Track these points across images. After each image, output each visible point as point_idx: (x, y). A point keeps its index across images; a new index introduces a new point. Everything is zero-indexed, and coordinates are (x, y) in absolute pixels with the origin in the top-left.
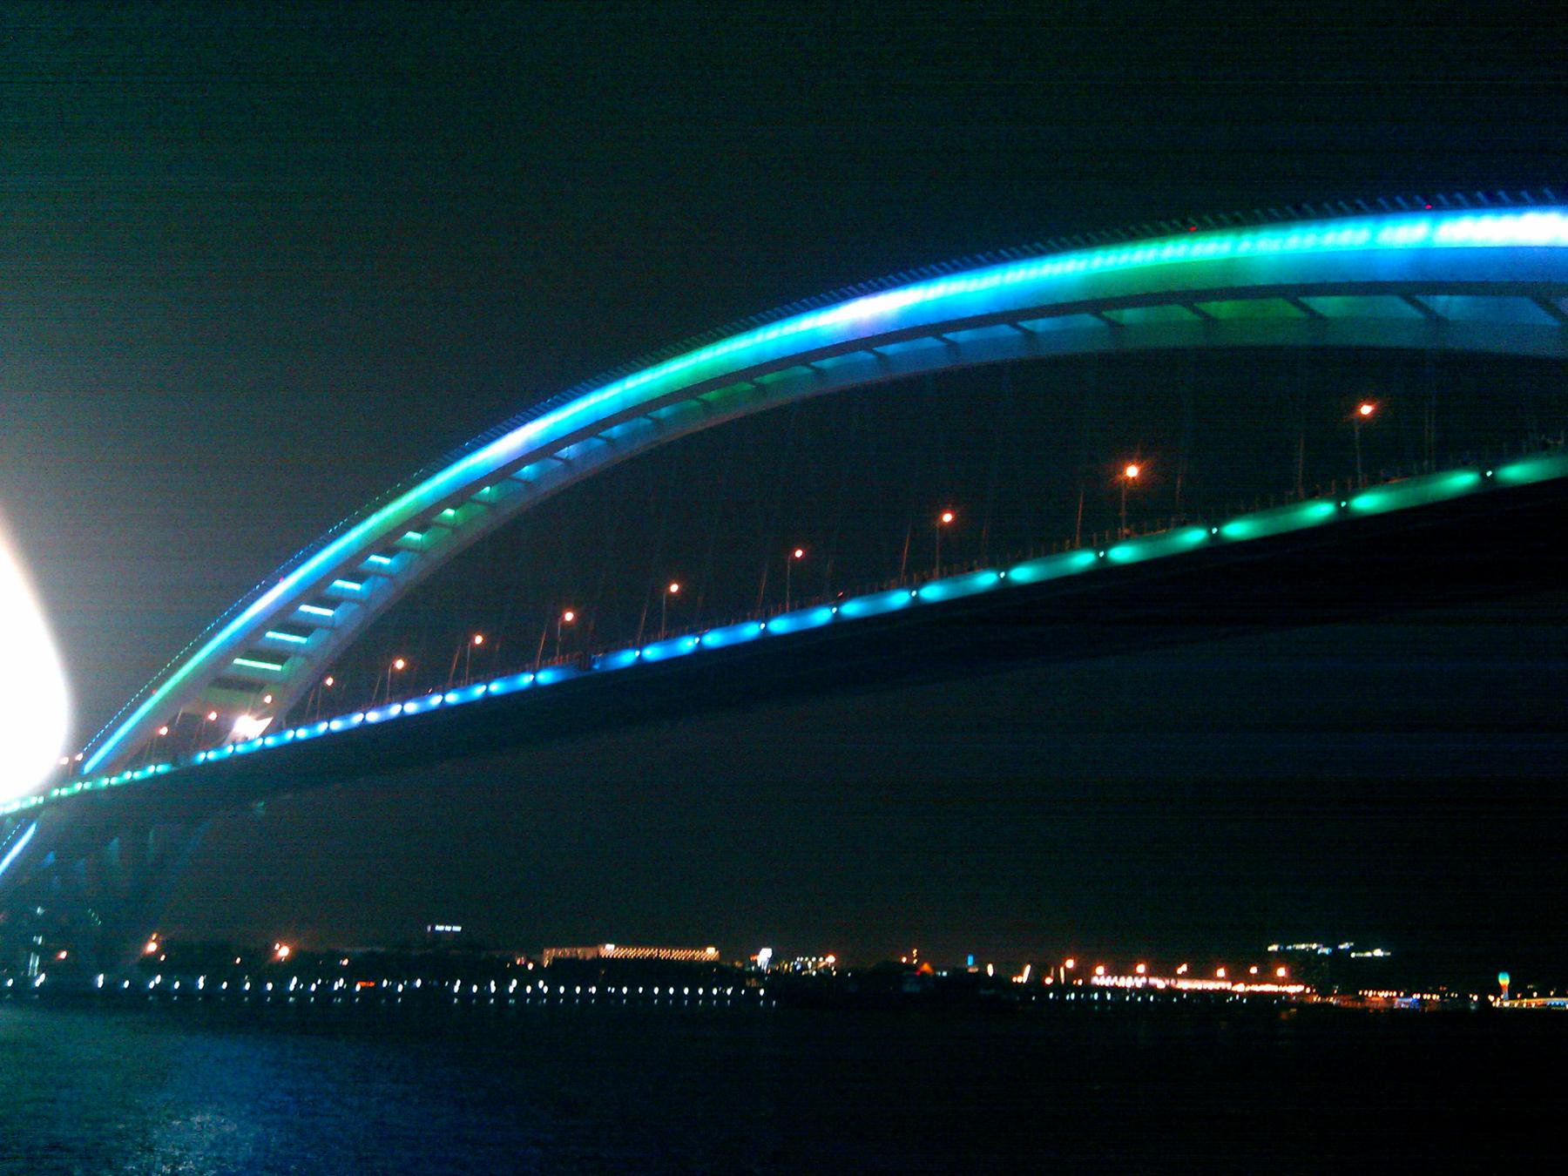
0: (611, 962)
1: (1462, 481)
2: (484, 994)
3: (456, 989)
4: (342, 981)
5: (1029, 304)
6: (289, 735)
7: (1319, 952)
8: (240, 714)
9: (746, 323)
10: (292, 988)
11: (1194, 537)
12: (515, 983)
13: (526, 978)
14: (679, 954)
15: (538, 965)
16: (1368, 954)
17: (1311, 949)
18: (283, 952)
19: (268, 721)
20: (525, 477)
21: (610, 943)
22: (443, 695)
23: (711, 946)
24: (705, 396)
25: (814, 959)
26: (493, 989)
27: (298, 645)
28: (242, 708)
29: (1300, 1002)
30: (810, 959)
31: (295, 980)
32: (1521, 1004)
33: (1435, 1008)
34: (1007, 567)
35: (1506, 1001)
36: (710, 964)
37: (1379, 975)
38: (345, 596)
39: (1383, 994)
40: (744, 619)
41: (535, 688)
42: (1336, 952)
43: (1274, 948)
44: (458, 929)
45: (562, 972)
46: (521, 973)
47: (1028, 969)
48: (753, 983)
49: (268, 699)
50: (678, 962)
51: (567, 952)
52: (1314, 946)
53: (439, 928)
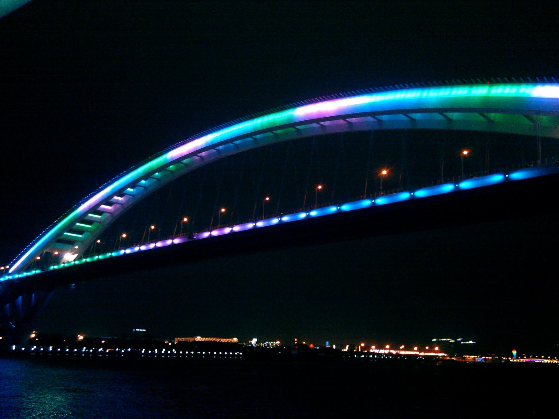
2: (153, 353)
3: (143, 352)
6: (84, 260)
10: (84, 351)
12: (164, 350)
13: (169, 348)
15: (173, 343)
16: (467, 343)
18: (81, 338)
21: (235, 337)
26: (156, 352)
27: (88, 228)
28: (67, 251)
29: (443, 359)
31: (85, 348)
33: (490, 362)
34: (309, 212)
35: (515, 359)
37: (471, 350)
38: (105, 211)
40: (248, 222)
41: (173, 245)
42: (456, 341)
43: (434, 340)
45: (181, 346)
47: (347, 347)
49: (77, 247)
51: (183, 339)
52: (449, 340)
53: (137, 330)
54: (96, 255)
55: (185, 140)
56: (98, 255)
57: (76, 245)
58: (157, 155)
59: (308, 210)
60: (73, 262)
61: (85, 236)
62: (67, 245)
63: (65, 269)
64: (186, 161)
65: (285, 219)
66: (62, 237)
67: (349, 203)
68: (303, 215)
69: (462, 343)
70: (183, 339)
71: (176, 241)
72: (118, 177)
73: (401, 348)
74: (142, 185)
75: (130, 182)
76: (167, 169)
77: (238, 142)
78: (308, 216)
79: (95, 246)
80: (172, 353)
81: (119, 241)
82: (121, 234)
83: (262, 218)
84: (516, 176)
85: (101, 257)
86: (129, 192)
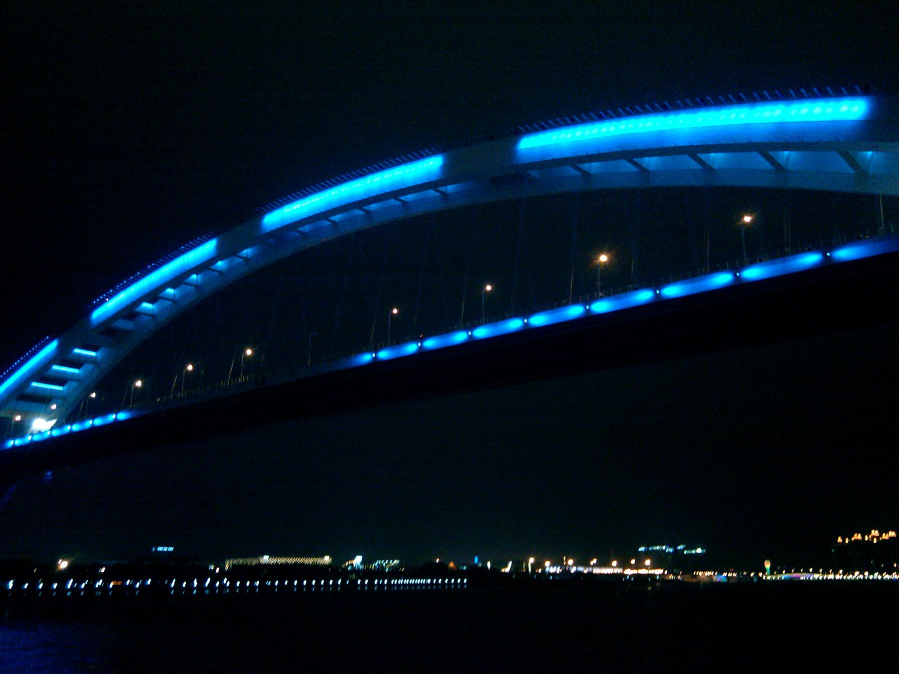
0: (267, 566)
1: (811, 259)
3: (173, 585)
4: (101, 581)
5: (591, 151)
6: (68, 428)
7: (667, 551)
8: (38, 417)
9: (361, 173)
11: (644, 296)
13: (216, 577)
14: (309, 561)
16: (693, 552)
17: (662, 550)
18: (63, 564)
19: (53, 422)
20: (219, 269)
22: (93, 421)
23: (328, 555)
24: (333, 218)
25: (387, 561)
27: (73, 374)
28: (37, 414)
30: (385, 562)
32: (776, 578)
33: (734, 581)
34: (422, 340)
36: (325, 567)
39: (708, 574)
41: (116, 422)
42: (676, 550)
43: (642, 549)
44: (171, 549)
45: (235, 573)
46: (212, 574)
47: (510, 564)
48: (354, 576)
49: (54, 407)
50: (308, 566)
51: (241, 561)
52: (664, 548)
54: (88, 418)
55: (333, 180)
56: (93, 419)
57: (53, 404)
58: (196, 243)
59: (471, 325)
60: (49, 433)
61: (69, 389)
62: (34, 405)
63: (33, 444)
64: (247, 252)
65: (430, 343)
66: (27, 391)
67: (491, 324)
68: (460, 337)
69: (685, 552)
70: (241, 561)
71: (122, 416)
72: (126, 283)
73: (592, 563)
74: (167, 297)
75: (147, 291)
76: (213, 267)
77: (337, 218)
78: (471, 337)
79: (87, 405)
80: (222, 586)
81: (130, 393)
82: (133, 382)
83: (579, 301)
84: (844, 254)
85: (98, 422)
86: (146, 309)
